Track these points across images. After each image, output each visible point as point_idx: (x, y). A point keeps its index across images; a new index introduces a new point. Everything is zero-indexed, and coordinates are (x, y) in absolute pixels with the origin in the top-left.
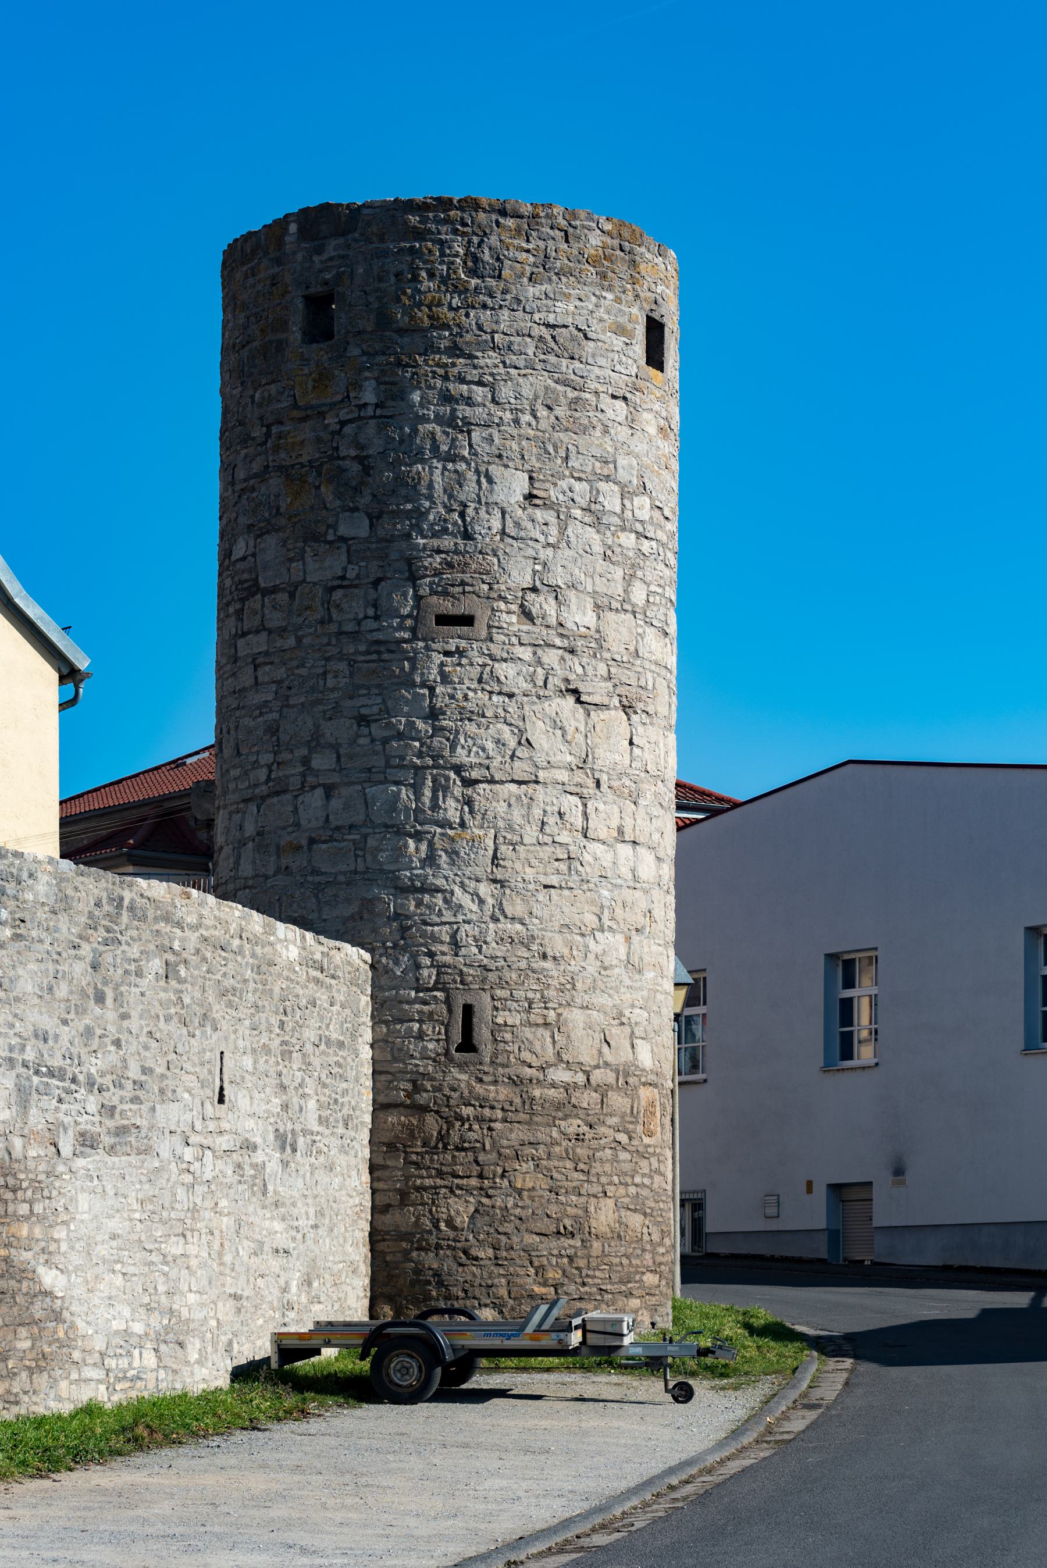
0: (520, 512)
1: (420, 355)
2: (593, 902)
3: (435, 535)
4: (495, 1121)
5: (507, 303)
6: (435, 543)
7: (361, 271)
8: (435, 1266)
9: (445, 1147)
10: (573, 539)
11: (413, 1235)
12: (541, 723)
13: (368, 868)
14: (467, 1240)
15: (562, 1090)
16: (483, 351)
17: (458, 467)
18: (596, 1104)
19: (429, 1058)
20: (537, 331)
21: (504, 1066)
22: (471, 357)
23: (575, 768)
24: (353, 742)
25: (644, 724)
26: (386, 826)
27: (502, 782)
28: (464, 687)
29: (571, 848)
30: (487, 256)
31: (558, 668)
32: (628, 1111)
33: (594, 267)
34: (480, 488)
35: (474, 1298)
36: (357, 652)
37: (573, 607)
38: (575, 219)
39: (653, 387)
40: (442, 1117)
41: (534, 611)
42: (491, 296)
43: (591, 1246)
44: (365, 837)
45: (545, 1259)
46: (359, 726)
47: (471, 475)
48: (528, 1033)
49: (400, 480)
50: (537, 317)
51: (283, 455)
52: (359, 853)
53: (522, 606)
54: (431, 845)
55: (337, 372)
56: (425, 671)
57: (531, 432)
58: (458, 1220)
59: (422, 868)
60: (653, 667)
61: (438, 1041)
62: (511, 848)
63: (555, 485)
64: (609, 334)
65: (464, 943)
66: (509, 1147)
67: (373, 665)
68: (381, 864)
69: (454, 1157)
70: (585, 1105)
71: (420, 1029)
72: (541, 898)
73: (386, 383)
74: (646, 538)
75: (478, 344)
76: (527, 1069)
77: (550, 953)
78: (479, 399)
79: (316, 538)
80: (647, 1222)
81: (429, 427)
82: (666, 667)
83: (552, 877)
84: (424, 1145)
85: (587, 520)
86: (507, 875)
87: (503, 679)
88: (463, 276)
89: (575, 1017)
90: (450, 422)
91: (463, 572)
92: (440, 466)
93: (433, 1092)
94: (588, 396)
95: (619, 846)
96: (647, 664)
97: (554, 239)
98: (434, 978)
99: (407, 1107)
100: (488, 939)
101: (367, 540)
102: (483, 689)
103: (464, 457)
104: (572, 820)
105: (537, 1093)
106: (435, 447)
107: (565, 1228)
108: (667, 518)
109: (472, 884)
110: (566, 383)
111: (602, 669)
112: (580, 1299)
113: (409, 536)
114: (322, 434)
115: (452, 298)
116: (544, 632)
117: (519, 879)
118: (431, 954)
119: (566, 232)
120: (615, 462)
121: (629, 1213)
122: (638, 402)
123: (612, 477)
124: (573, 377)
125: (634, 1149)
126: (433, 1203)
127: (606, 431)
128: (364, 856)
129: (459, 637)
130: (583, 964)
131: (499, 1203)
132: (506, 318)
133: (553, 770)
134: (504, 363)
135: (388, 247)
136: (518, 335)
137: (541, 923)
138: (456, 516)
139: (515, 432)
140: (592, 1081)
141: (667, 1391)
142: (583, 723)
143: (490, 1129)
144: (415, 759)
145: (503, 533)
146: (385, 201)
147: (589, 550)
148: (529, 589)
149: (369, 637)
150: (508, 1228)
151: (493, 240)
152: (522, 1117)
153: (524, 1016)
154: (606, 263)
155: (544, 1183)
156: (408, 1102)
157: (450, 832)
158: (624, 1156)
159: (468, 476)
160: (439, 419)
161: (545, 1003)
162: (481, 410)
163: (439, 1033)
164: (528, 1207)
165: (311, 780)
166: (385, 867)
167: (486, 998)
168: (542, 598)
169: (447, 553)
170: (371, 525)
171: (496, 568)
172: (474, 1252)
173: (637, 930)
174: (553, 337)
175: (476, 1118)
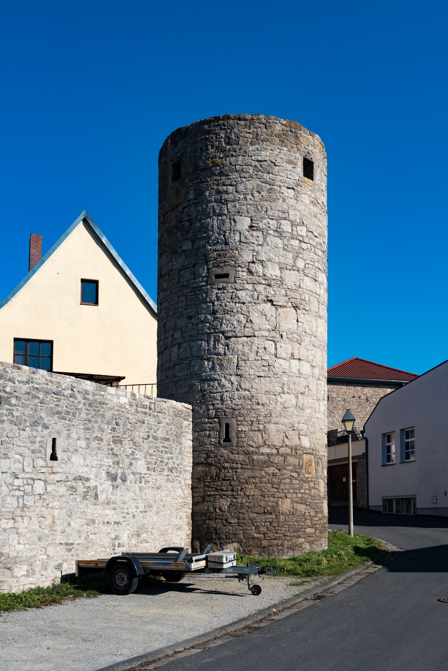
0: (247, 233)
1: (209, 177)
2: (279, 382)
3: (215, 245)
4: (238, 468)
5: (241, 153)
6: (214, 247)
7: (189, 150)
8: (215, 526)
9: (218, 479)
10: (269, 242)
11: (207, 514)
12: (256, 313)
13: (191, 373)
14: (227, 516)
15: (266, 456)
16: (232, 173)
17: (223, 218)
18: (282, 461)
19: (212, 445)
20: (253, 163)
21: (241, 447)
22: (228, 175)
23: (271, 330)
24: (186, 326)
25: (304, 314)
26: (198, 357)
27: (240, 337)
28: (225, 301)
29: (269, 361)
30: (233, 136)
31: (263, 292)
32: (297, 464)
33: (278, 138)
34: (231, 225)
35: (230, 539)
36: (188, 292)
37: (270, 268)
38: (269, 119)
39: (307, 185)
40: (217, 468)
41: (253, 270)
42: (235, 152)
43: (280, 518)
44: (190, 361)
45: (259, 523)
46: (188, 320)
47: (228, 221)
48: (251, 434)
49: (202, 226)
50: (253, 158)
51: (167, 225)
52: (188, 368)
53: (248, 269)
54: (213, 363)
55: (182, 190)
56: (211, 296)
57: (251, 202)
58: (223, 508)
59: (210, 372)
60: (308, 292)
61: (216, 438)
62: (244, 362)
63: (262, 221)
64: (285, 163)
65: (225, 400)
66: (243, 479)
67: (193, 296)
68: (195, 371)
69: (222, 483)
70: (276, 462)
71: (209, 434)
72: (256, 381)
73: (197, 190)
74: (304, 242)
75: (230, 170)
76: (251, 448)
77: (260, 402)
78: (231, 191)
79: (175, 252)
80: (308, 508)
81: (212, 204)
82: (316, 293)
83: (261, 373)
84: (211, 478)
85: (276, 235)
86: (242, 373)
87: (240, 297)
88: (224, 145)
89: (272, 427)
90: (220, 201)
91: (225, 257)
92: (216, 218)
93: (214, 458)
94: (276, 187)
95: (292, 360)
96: (305, 291)
97: (260, 128)
98: (214, 413)
99: (205, 464)
100: (235, 398)
101: (191, 250)
102: (233, 302)
103: (225, 214)
104: (270, 350)
105: (255, 457)
106: (214, 212)
107: (268, 511)
108: (316, 237)
109: (229, 377)
110: (266, 183)
111: (283, 292)
112: (275, 539)
113: (205, 246)
114: (178, 214)
115: (220, 154)
116: (257, 278)
117: (247, 374)
118: (213, 405)
119: (265, 124)
120: (288, 213)
121: (298, 504)
122: (299, 190)
123: (287, 219)
124: (269, 180)
125: (300, 479)
126: (214, 501)
127: (284, 200)
128: (190, 369)
129: (223, 282)
130: (275, 406)
131: (239, 501)
132: (241, 159)
133: (261, 331)
134: (240, 176)
135: (198, 140)
136: (246, 165)
137: (257, 391)
138: (222, 236)
139: (245, 203)
140: (280, 452)
141: (249, 589)
142: (275, 313)
143: (236, 472)
144: (207, 331)
145: (240, 241)
146: (197, 122)
147: (276, 246)
148: (251, 262)
149: (191, 286)
150: (243, 511)
151: (236, 130)
152: (249, 467)
153: (250, 427)
154: (284, 136)
155: (258, 493)
156: (205, 462)
157: (220, 357)
158: (295, 482)
159: (226, 221)
160: (216, 201)
161: (258, 422)
162: (231, 195)
163: (216, 435)
164: (251, 502)
165: (174, 342)
166: (197, 372)
167: (234, 421)
168: (256, 265)
169: (219, 251)
170: (192, 244)
171: (237, 255)
172: (229, 520)
173: (302, 393)
174: (261, 165)
175: (230, 467)
